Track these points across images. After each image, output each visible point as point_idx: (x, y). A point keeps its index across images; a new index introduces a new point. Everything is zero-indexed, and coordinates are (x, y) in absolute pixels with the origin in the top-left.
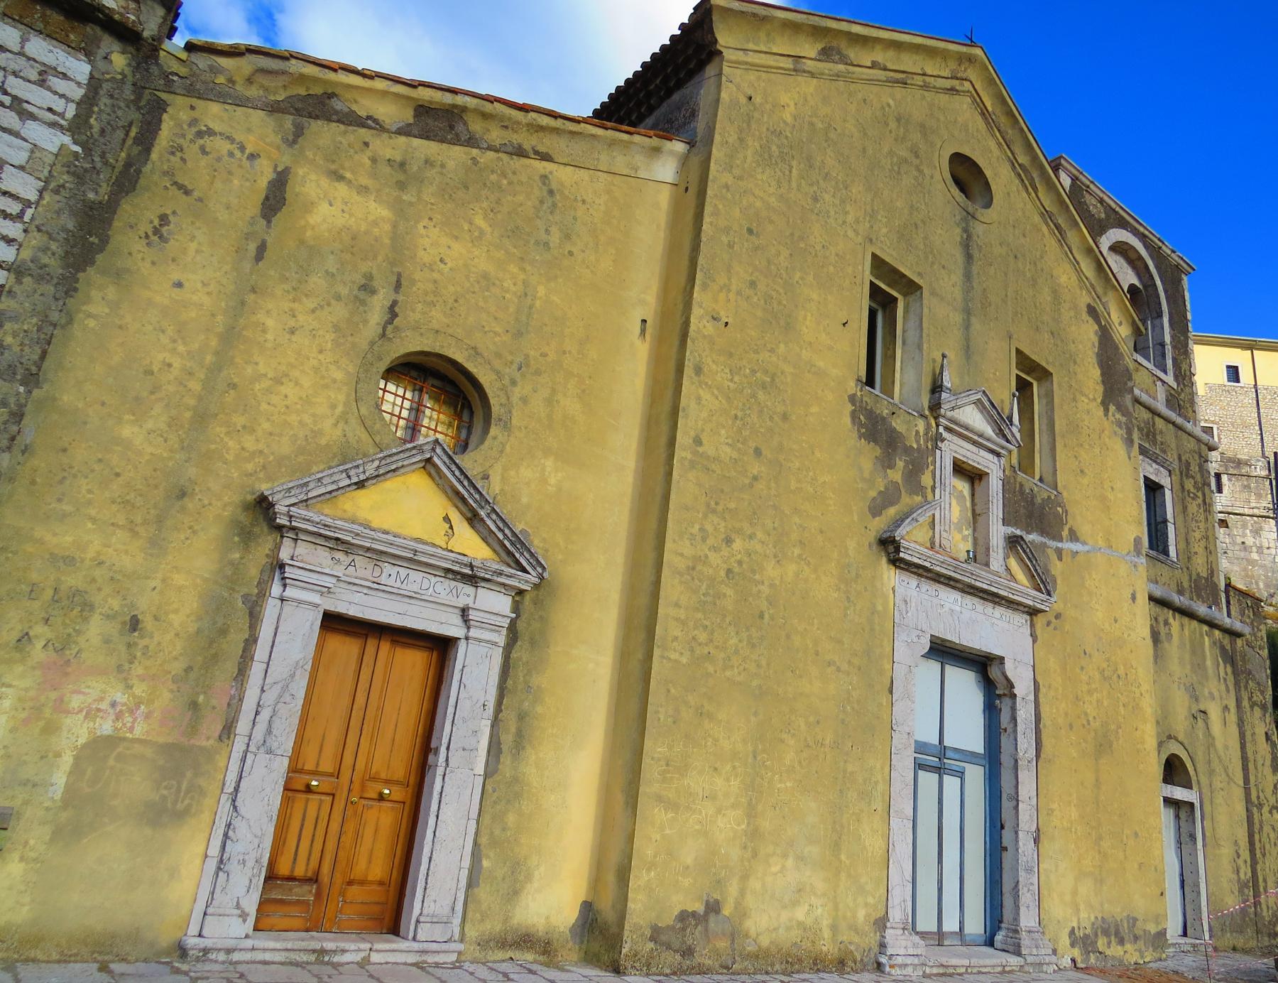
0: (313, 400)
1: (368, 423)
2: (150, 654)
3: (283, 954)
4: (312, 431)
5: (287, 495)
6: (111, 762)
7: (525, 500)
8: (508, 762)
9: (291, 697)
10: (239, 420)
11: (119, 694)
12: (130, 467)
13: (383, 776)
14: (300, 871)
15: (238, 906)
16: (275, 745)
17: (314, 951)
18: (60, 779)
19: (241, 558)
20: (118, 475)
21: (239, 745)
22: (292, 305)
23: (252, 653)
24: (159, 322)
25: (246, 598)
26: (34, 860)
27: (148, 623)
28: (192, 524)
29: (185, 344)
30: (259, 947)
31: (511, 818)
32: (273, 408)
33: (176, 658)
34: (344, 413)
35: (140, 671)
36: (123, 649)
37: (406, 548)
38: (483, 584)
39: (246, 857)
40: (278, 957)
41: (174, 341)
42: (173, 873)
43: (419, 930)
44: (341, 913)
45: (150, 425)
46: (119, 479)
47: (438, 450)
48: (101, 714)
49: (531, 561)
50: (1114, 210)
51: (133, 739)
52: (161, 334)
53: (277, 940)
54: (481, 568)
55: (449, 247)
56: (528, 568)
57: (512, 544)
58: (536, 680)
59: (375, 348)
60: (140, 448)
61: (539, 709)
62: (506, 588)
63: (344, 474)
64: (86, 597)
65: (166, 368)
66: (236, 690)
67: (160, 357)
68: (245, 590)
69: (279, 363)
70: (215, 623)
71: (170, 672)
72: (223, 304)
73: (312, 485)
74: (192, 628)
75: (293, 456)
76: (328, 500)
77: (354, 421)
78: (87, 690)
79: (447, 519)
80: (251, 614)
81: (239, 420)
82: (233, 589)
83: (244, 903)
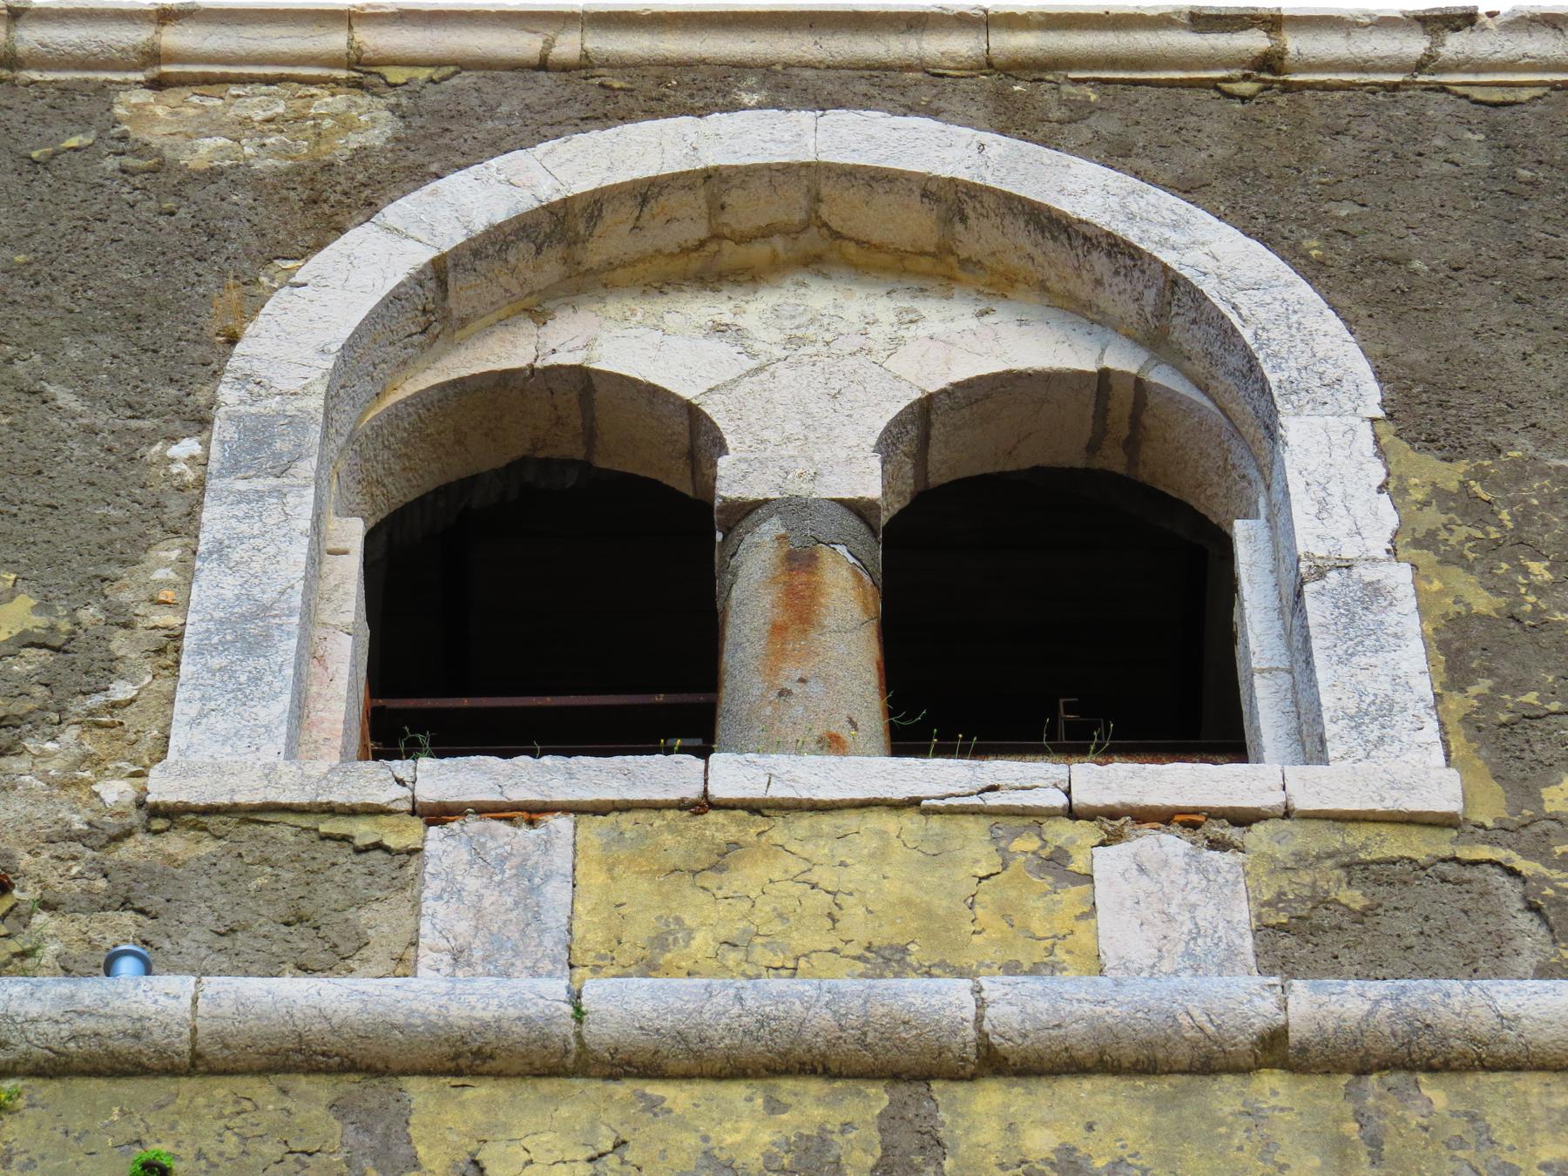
50: (543, 65)
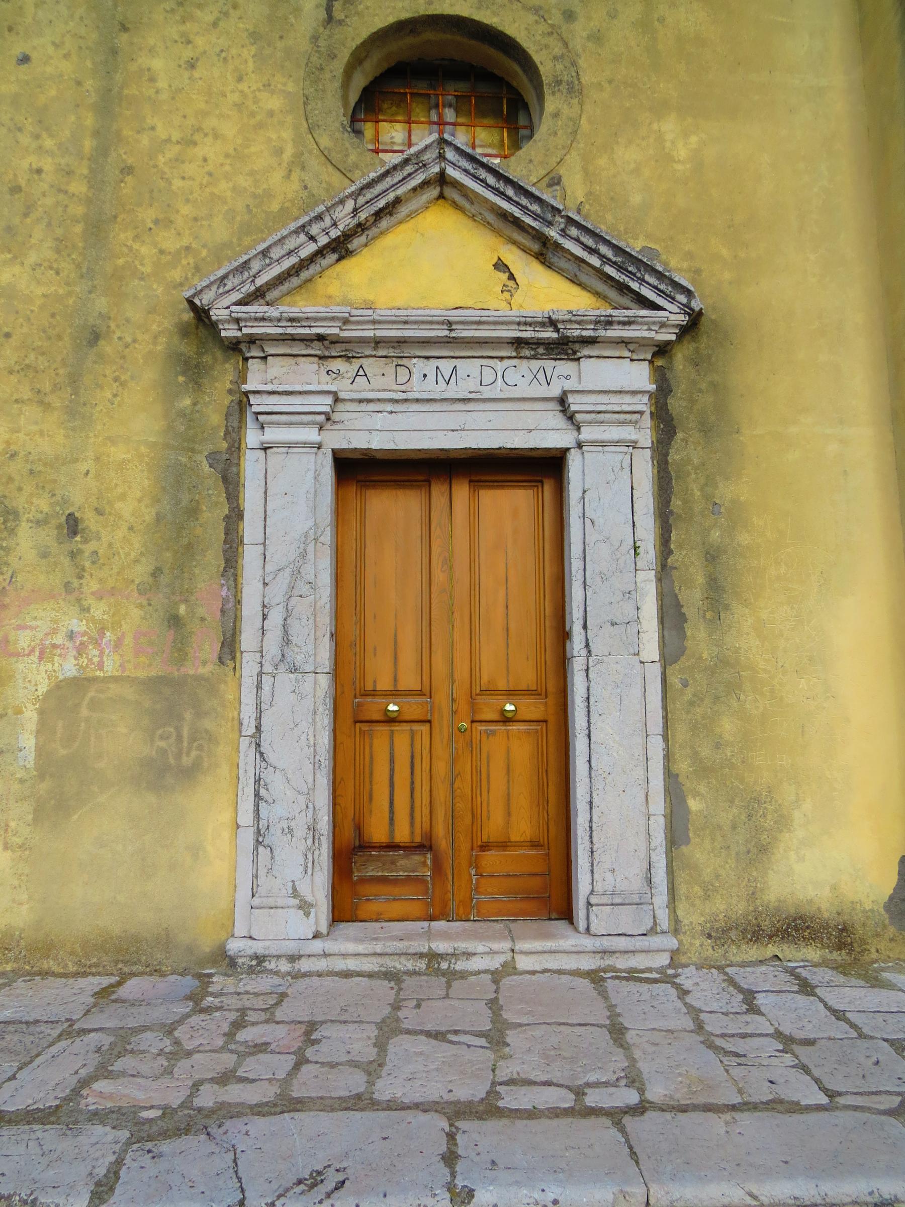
0: (246, 151)
1: (335, 157)
2: (101, 561)
3: (374, 960)
4: (255, 196)
5: (221, 290)
6: (84, 712)
7: (636, 199)
8: (702, 634)
9: (308, 586)
10: (148, 215)
11: (75, 621)
12: (21, 320)
13: (502, 685)
14: (402, 835)
15: (295, 893)
16: (300, 658)
17: (421, 956)
18: (28, 741)
19: (195, 404)
20: (8, 335)
21: (249, 667)
22: (182, 28)
23: (240, 534)
24: (12, 119)
25: (212, 458)
26: (20, 847)
27: (90, 520)
28: (117, 373)
29: (51, 136)
30: (332, 952)
31: (727, 726)
32: (190, 183)
33: (137, 561)
34: (298, 155)
35: (94, 586)
36: (66, 561)
37: (431, 323)
38: (586, 351)
39: (293, 824)
40: (369, 965)
41: (37, 137)
42: (196, 850)
43: (593, 917)
44: (478, 893)
45: (32, 258)
46: (11, 340)
47: (450, 154)
48: (58, 651)
49: (662, 287)
51: (105, 677)
52: (18, 134)
53: (358, 940)
54: (570, 321)
56: (660, 301)
57: (620, 268)
58: (726, 491)
59: (322, 43)
60: (27, 292)
61: (744, 538)
62: (631, 347)
63: (302, 237)
64: (7, 502)
65: (36, 177)
66: (228, 589)
67: (25, 164)
68: (209, 448)
69: (185, 117)
70: (178, 503)
71: (133, 581)
72: (89, 64)
73: (256, 266)
74: (149, 515)
75: (235, 240)
76: (300, 286)
77: (315, 163)
78: (34, 623)
79: (500, 266)
80: (225, 479)
81: (148, 215)
82: (193, 450)
83: (304, 889)
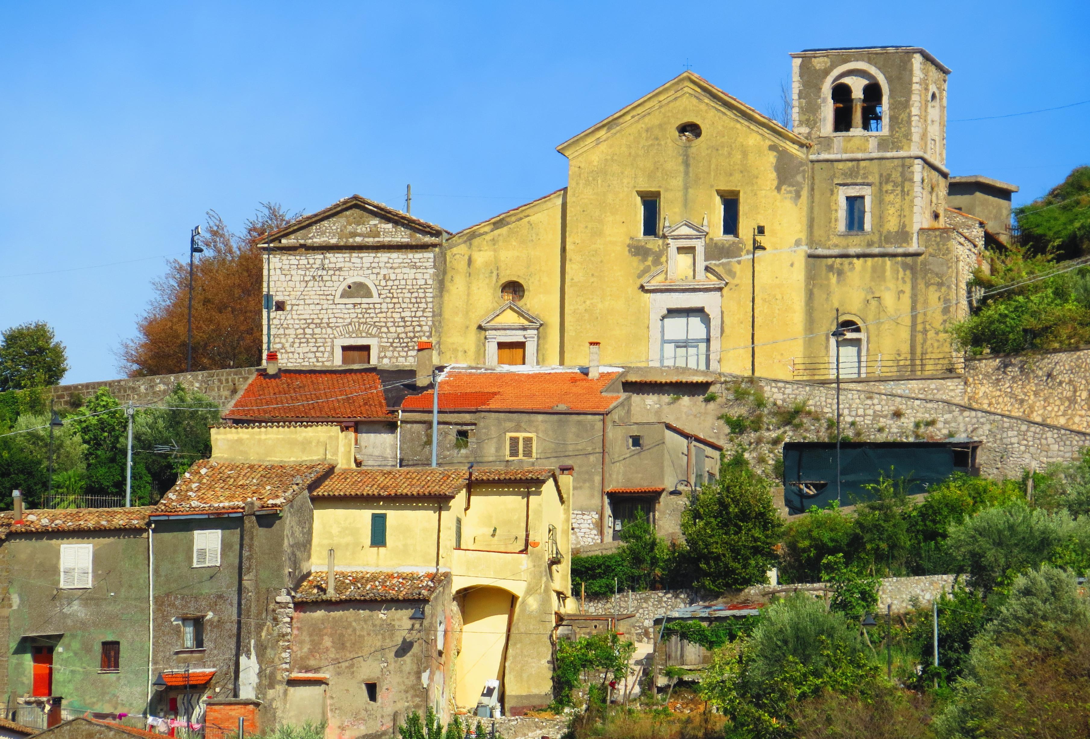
55: (792, 265)
